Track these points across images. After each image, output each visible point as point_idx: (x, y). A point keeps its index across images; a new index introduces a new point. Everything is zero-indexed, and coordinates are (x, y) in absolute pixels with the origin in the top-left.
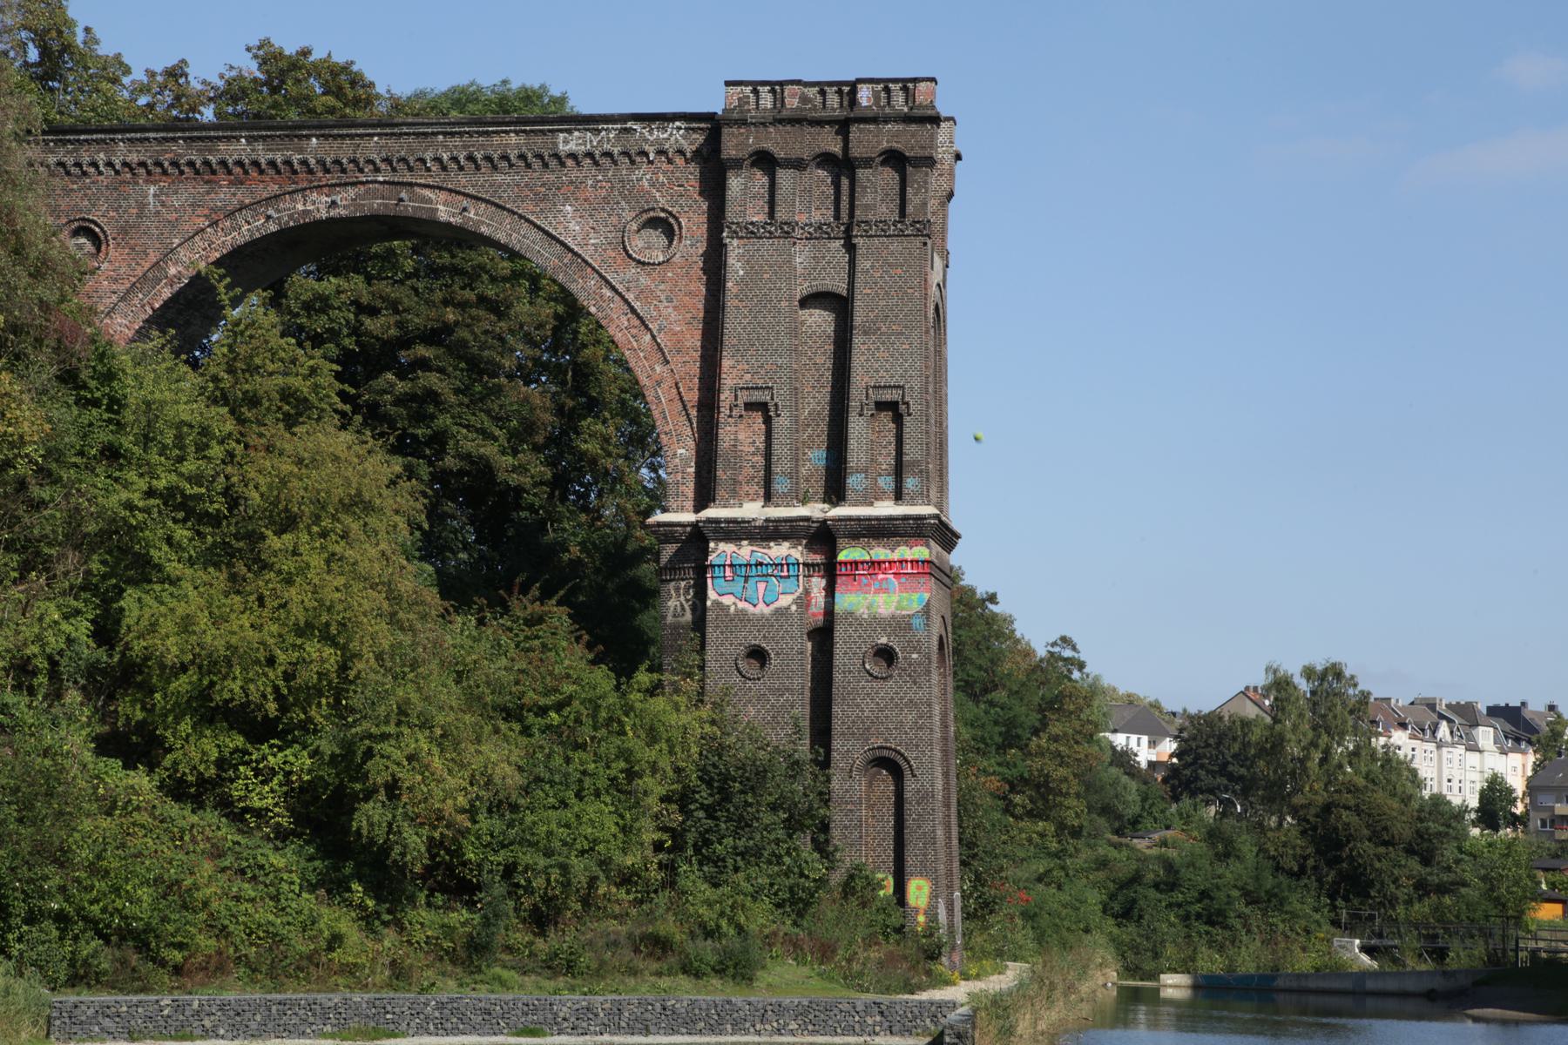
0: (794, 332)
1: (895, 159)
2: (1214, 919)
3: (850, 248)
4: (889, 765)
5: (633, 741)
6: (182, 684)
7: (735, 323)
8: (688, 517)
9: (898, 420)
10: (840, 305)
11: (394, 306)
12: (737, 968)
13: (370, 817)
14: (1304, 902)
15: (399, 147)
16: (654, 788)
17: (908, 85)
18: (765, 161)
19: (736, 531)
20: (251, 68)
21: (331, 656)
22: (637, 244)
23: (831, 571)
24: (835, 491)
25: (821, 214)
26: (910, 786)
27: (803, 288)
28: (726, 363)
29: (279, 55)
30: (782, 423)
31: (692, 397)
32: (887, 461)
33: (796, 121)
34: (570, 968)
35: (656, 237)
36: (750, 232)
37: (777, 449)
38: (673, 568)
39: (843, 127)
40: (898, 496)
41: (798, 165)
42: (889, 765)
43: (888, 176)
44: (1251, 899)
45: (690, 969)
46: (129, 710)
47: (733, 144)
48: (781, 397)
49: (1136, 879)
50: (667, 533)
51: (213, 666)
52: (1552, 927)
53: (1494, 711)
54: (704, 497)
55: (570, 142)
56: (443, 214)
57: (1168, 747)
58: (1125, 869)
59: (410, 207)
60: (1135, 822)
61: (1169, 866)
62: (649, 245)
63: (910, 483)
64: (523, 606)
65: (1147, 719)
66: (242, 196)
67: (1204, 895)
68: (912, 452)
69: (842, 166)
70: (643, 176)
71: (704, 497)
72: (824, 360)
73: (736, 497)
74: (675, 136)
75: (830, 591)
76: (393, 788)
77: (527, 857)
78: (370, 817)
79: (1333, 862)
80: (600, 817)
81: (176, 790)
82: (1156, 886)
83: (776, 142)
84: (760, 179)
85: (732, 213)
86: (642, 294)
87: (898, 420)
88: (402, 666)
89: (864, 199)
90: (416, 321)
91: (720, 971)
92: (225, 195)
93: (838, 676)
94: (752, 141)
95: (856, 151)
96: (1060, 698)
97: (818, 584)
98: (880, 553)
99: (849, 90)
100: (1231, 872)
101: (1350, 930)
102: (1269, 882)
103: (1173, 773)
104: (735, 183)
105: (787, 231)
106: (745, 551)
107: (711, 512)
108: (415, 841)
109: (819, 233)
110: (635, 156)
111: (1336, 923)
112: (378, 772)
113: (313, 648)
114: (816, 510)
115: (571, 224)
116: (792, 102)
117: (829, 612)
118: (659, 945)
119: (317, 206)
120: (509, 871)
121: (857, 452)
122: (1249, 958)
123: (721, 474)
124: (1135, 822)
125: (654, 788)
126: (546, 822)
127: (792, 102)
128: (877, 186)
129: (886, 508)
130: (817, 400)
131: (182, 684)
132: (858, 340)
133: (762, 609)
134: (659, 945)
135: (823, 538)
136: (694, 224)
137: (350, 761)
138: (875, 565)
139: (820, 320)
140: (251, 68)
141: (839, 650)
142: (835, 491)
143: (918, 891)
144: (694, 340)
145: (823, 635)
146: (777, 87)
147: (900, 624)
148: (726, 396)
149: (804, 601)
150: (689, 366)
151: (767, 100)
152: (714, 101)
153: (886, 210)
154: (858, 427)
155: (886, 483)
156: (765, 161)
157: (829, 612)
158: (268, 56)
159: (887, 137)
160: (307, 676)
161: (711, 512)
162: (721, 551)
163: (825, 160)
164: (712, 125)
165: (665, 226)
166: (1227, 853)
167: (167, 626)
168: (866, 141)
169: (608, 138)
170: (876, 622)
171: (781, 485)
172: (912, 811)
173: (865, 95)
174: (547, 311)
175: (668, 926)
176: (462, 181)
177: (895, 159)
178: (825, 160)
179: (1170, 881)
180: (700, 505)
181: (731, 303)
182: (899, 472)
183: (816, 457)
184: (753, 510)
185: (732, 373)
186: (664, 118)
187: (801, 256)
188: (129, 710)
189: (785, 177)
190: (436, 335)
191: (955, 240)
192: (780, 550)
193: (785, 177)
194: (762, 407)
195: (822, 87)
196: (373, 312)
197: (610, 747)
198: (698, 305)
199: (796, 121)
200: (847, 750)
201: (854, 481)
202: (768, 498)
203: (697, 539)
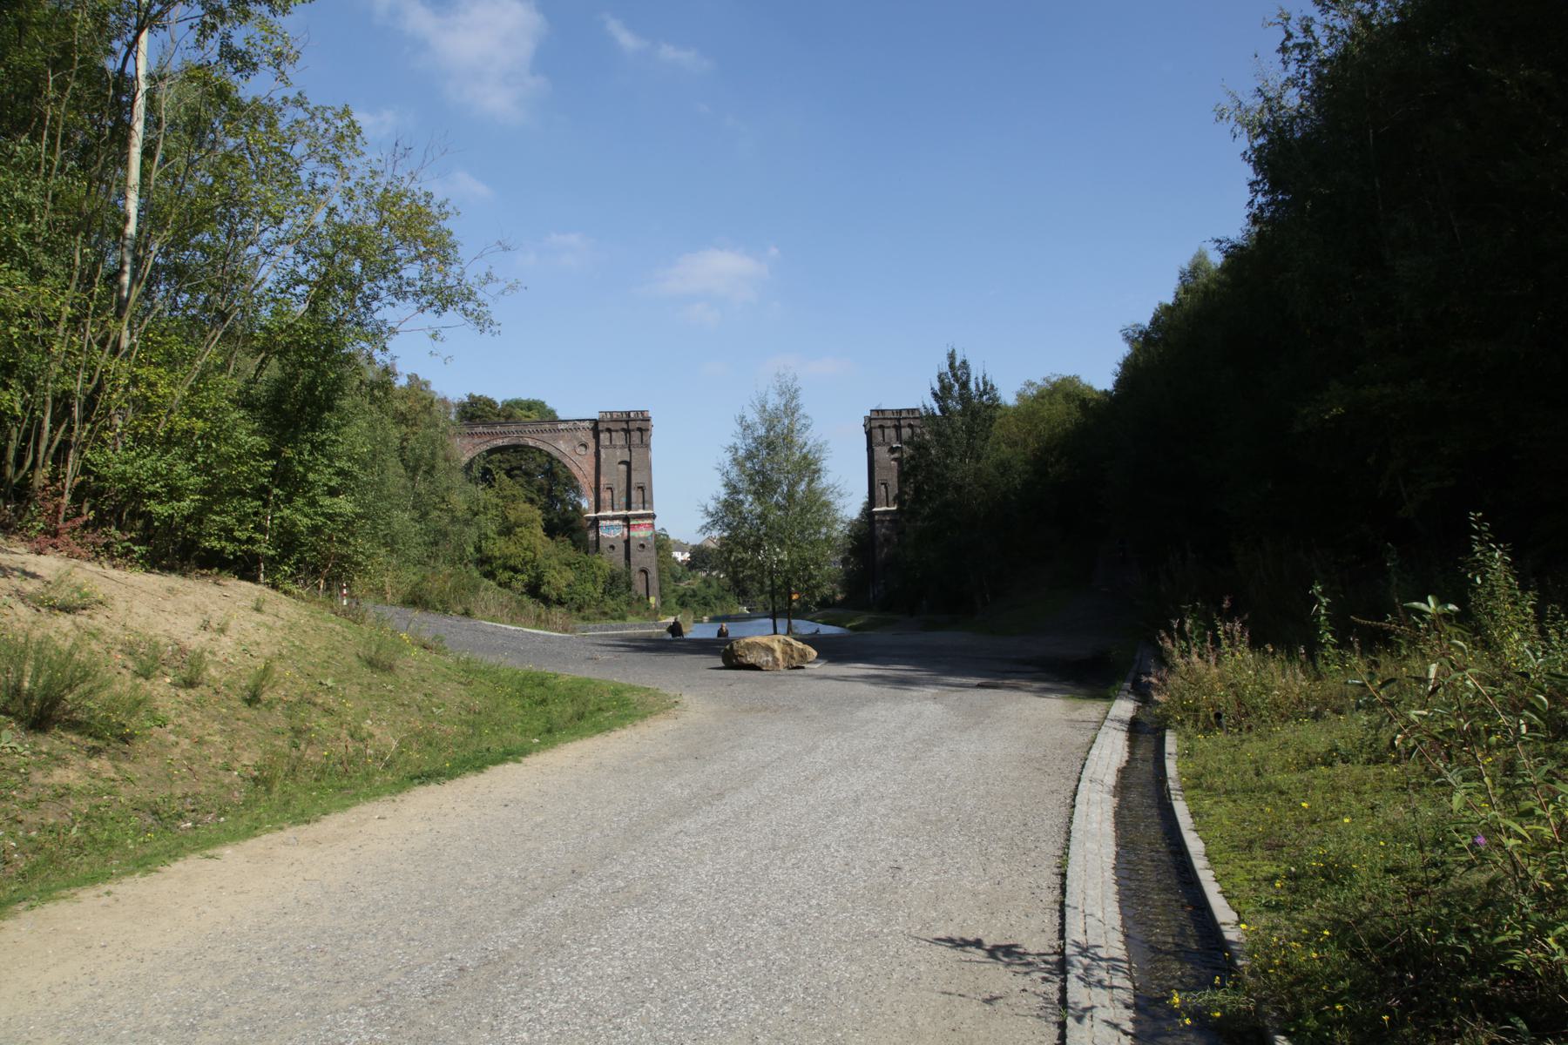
0: (618, 470)
1: (640, 429)
2: (707, 604)
3: (630, 450)
4: (644, 571)
5: (595, 570)
6: (500, 562)
7: (603, 469)
8: (594, 515)
9: (643, 491)
10: (628, 464)
11: (509, 461)
12: (623, 618)
13: (544, 589)
14: (731, 598)
15: (519, 428)
16: (600, 580)
17: (642, 412)
18: (609, 430)
19: (606, 518)
20: (466, 400)
21: (532, 554)
22: (578, 450)
23: (629, 527)
24: (629, 507)
25: (623, 443)
26: (649, 576)
27: (619, 460)
28: (602, 478)
29: (474, 397)
30: (616, 492)
31: (593, 486)
32: (641, 500)
33: (616, 421)
34: (588, 619)
35: (583, 448)
36: (606, 447)
37: (615, 499)
38: (590, 527)
39: (627, 422)
40: (644, 508)
41: (617, 431)
42: (644, 571)
43: (639, 433)
44: (716, 598)
45: (613, 618)
46: (487, 568)
47: (601, 427)
48: (615, 486)
49: (685, 594)
50: (588, 519)
51: (507, 558)
52: (342, 602)
54: (597, 510)
55: (561, 426)
56: (531, 444)
57: (687, 555)
58: (681, 592)
59: (522, 442)
60: (680, 578)
61: (693, 590)
62: (581, 450)
63: (647, 505)
64: (559, 538)
65: (681, 547)
66: (481, 440)
67: (704, 598)
68: (646, 498)
69: (627, 431)
70: (579, 434)
71: (597, 510)
72: (624, 476)
73: (605, 509)
74: (587, 424)
75: (629, 531)
76: (549, 583)
77: (576, 596)
78: (544, 589)
79: (738, 587)
80: (589, 586)
81: (500, 585)
82: (690, 596)
83: (611, 426)
84: (608, 435)
85: (602, 443)
86: (580, 462)
87: (643, 491)
88: (548, 557)
89: (633, 439)
90: (514, 464)
91: (619, 618)
92: (476, 440)
93: (631, 551)
94: (606, 426)
95: (631, 428)
96: (662, 545)
97: (626, 530)
98: (640, 522)
99: (628, 414)
100: (710, 591)
101: (743, 605)
102: (721, 593)
103: (689, 563)
104: (602, 436)
105: (615, 447)
106: (608, 523)
107: (600, 514)
108: (554, 593)
109: (622, 447)
110: (577, 429)
111: (739, 603)
112: (545, 580)
113: (528, 553)
114: (624, 512)
115: (562, 445)
116: (615, 416)
117: (629, 536)
118: (605, 614)
119: (499, 442)
120: (572, 599)
121: (634, 498)
122: (719, 613)
123: (602, 504)
124: (680, 578)
125: (600, 580)
126: (579, 588)
127: (615, 416)
128: (636, 436)
129: (641, 512)
130: (623, 486)
131: (500, 562)
132: (633, 472)
133: (613, 536)
134: (605, 614)
135: (626, 519)
136: (592, 445)
137: (539, 577)
138: (639, 525)
139: (623, 467)
140: (466, 400)
141: (632, 545)
142: (629, 507)
143: (652, 600)
144: (593, 472)
145: (627, 542)
146: (611, 413)
147: (646, 539)
148: (602, 486)
149: (622, 534)
150: (592, 479)
151: (609, 416)
152: (596, 416)
153: (638, 441)
154: (634, 493)
155: (641, 505)
156: (609, 430)
157: (629, 536)
158: (471, 396)
159: (638, 424)
160: (527, 559)
161: (600, 514)
162: (602, 523)
163: (623, 430)
164: (596, 422)
165: (585, 446)
166: (709, 586)
167: (496, 549)
168: (633, 425)
169: (570, 425)
170: (640, 538)
171: (616, 507)
172: (650, 582)
173: (632, 415)
174: (545, 459)
175: (607, 610)
176: (535, 436)
177: (640, 429)
178: (623, 430)
179: (694, 594)
180: (596, 512)
181: (602, 464)
182: (644, 502)
183: (624, 500)
184: (609, 513)
185: (603, 480)
186: (584, 420)
187: (618, 452)
188: (487, 568)
189: (614, 434)
190: (519, 468)
191: (652, 446)
192: (617, 522)
193: (614, 434)
194: (611, 489)
195: (622, 413)
196: (504, 463)
197: (590, 572)
198: (594, 465)
199: (616, 421)
200: (635, 568)
201: (633, 506)
202: (613, 510)
203: (596, 521)
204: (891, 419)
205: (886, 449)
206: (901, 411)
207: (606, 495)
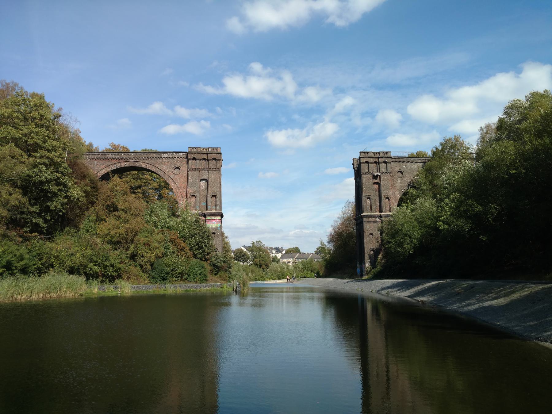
3: (208, 172)
41: (372, 163)
53: (275, 248)
69: (377, 163)
92: (108, 163)
98: (213, 218)
127: (199, 150)
169: (170, 155)
178: (376, 163)
204: (373, 158)
205: (370, 176)
206: (208, 148)
207: (385, 202)
